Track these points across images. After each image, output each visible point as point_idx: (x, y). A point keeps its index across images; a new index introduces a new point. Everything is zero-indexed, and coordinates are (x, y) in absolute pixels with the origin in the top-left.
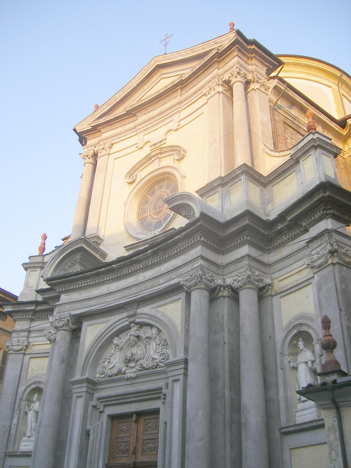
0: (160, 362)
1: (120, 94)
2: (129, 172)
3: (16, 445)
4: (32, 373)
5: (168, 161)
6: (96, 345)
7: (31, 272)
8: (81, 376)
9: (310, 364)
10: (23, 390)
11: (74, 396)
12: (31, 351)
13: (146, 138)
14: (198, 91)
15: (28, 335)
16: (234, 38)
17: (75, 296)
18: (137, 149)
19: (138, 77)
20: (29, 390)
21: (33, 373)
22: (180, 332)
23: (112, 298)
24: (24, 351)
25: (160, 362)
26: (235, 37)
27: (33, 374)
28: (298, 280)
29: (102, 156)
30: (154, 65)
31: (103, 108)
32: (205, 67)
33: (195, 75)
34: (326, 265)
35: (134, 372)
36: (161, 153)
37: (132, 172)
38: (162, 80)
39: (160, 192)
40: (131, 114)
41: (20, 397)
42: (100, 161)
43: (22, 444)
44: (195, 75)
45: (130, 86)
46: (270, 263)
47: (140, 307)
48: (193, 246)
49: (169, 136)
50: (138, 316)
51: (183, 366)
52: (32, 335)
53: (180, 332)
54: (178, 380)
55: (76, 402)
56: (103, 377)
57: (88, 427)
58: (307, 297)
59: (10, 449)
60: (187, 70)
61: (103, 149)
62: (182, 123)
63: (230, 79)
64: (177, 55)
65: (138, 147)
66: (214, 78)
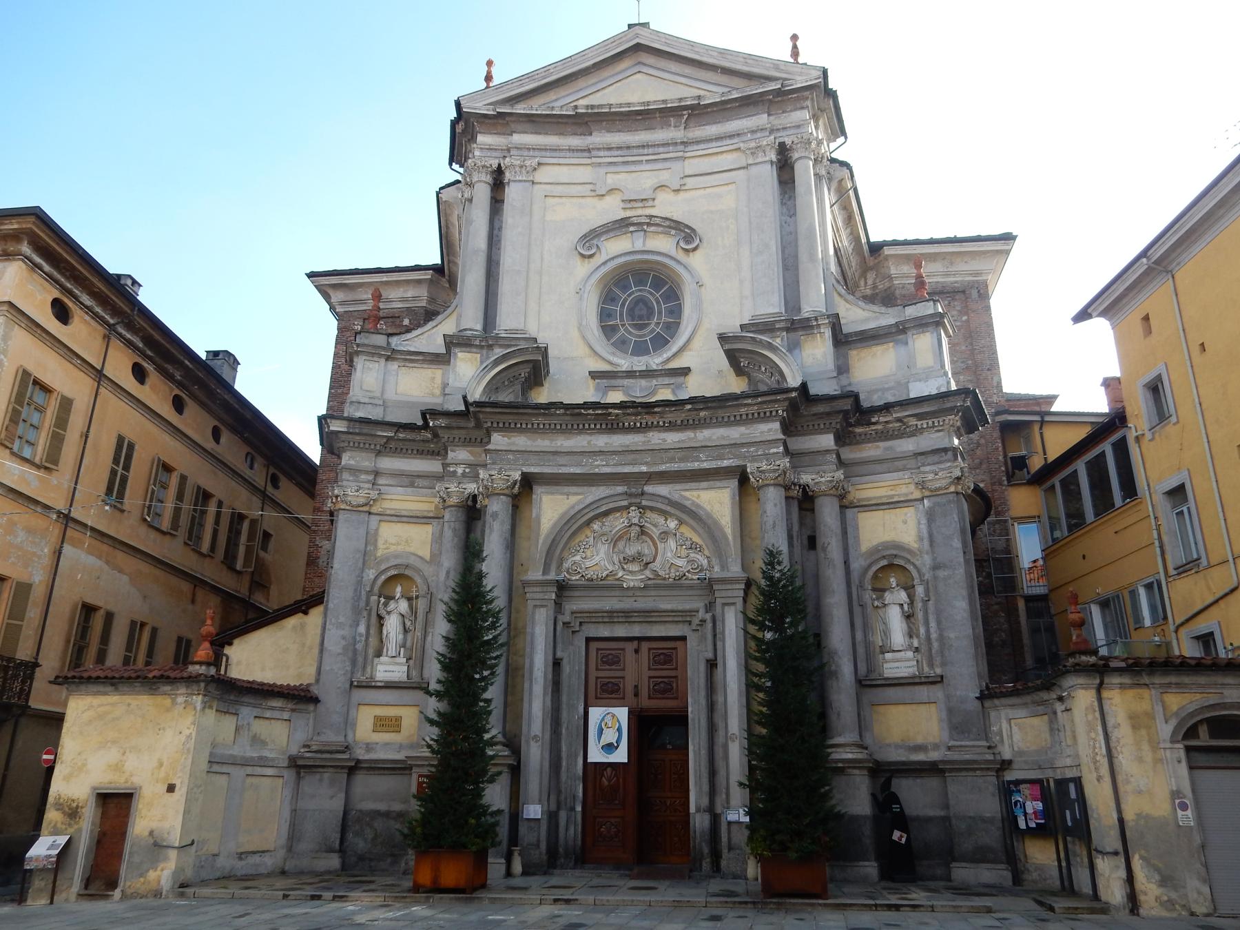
0: (688, 572)
1: (557, 69)
2: (585, 236)
3: (369, 669)
4: (385, 549)
5: (663, 244)
6: (566, 528)
7: (366, 362)
8: (544, 573)
9: (906, 607)
10: (372, 577)
11: (530, 603)
12: (380, 510)
13: (612, 180)
14: (725, 137)
15: (375, 479)
16: (816, 79)
17: (521, 441)
18: (593, 194)
19: (597, 50)
20: (383, 578)
21: (387, 548)
22: (730, 537)
23: (602, 460)
24: (366, 509)
25: (688, 572)
26: (819, 78)
27: (388, 551)
28: (892, 496)
29: (520, 181)
30: (631, 40)
31: (521, 82)
32: (748, 103)
33: (724, 109)
34: (945, 491)
35: (642, 580)
36: (648, 224)
37: (592, 237)
38: (638, 76)
39: (640, 290)
40: (583, 121)
41: (368, 590)
42: (513, 193)
43: (380, 668)
44: (724, 109)
45: (579, 60)
46: (794, 453)
47: (789, 512)
48: (764, 418)
49: (662, 197)
50: (645, 497)
51: (743, 586)
52: (381, 481)
53: (730, 537)
54: (734, 604)
55: (533, 613)
56: (577, 580)
57: (559, 654)
58: (905, 522)
59: (359, 677)
60: (712, 91)
61: (521, 167)
62: (691, 182)
63: (794, 146)
64: (687, 47)
65: (1161, 415)
66: (762, 130)
